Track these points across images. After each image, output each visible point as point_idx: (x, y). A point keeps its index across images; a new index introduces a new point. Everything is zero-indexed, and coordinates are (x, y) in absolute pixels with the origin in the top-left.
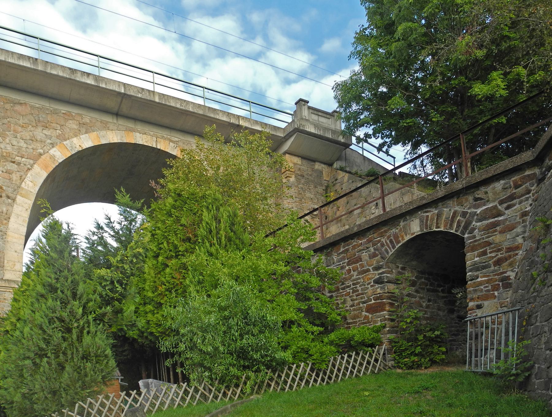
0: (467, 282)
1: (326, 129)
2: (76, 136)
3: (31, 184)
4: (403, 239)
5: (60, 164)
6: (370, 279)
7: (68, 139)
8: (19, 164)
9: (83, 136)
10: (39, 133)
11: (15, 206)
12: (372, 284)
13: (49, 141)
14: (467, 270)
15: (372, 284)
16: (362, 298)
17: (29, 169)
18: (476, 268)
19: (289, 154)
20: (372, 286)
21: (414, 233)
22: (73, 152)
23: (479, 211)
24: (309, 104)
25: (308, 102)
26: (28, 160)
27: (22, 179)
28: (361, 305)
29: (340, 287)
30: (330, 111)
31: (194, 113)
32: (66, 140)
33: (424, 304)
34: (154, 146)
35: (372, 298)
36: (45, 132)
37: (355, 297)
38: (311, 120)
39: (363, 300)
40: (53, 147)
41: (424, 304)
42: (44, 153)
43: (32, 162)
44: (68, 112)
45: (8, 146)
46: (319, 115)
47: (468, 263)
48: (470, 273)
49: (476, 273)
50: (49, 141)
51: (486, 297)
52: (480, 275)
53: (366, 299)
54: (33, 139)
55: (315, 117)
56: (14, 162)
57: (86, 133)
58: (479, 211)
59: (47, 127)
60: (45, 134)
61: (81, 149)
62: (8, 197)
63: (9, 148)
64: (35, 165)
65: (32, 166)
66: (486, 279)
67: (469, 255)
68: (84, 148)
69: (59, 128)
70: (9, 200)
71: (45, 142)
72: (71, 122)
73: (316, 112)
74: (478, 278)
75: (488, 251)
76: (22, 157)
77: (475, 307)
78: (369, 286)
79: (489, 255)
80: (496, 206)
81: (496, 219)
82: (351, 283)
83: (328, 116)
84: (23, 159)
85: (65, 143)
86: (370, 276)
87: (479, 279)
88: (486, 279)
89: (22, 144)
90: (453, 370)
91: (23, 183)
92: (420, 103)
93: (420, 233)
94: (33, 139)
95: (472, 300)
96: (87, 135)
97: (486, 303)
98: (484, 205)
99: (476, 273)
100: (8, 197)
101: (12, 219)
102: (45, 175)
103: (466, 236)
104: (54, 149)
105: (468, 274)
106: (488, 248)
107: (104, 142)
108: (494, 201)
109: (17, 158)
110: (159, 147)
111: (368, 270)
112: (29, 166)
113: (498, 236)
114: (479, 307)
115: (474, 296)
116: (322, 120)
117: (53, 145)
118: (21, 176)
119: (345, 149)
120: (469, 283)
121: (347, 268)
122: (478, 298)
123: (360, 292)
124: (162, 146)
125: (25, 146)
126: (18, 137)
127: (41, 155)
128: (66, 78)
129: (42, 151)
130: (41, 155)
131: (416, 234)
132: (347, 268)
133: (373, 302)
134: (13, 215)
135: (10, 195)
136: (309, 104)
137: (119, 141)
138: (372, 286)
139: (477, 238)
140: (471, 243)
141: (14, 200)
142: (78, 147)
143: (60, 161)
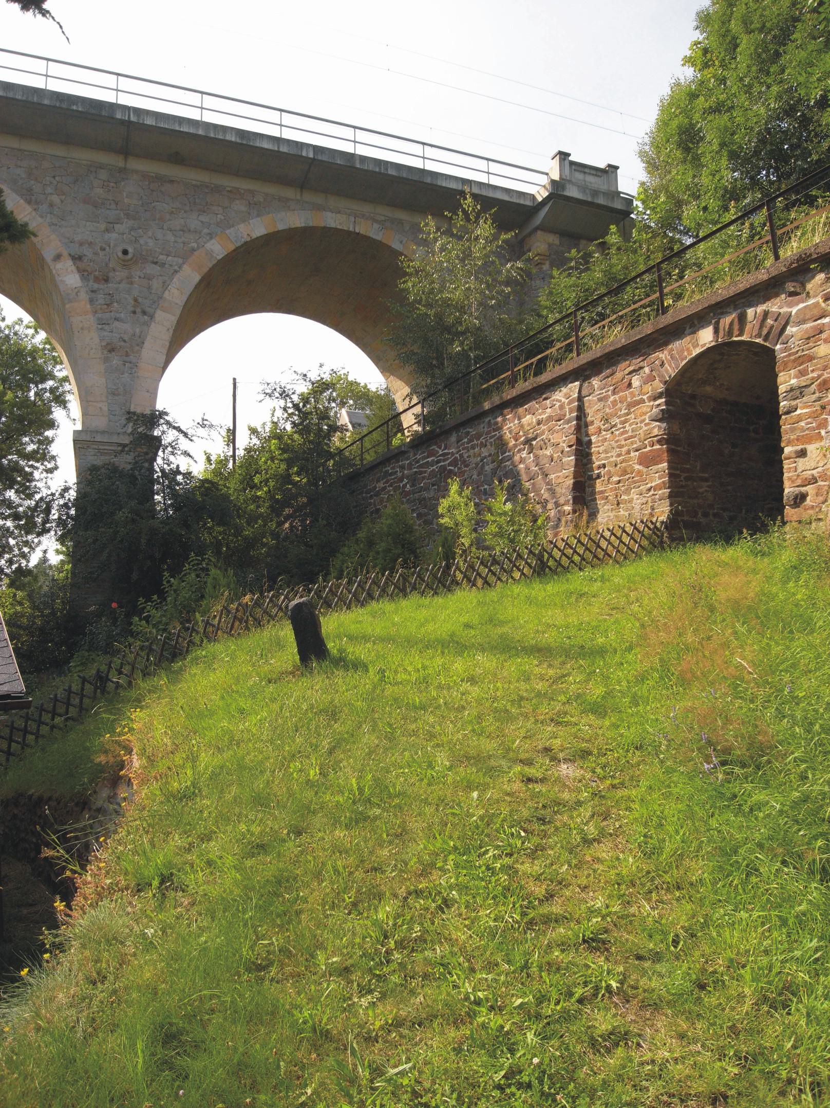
0: (780, 416)
1: (595, 193)
2: (244, 221)
3: (176, 293)
4: (690, 354)
5: (219, 261)
6: (645, 414)
7: (233, 226)
8: (163, 265)
9: (254, 220)
10: (194, 222)
11: (153, 324)
12: (647, 421)
13: (206, 231)
14: (781, 397)
15: (647, 421)
16: (632, 443)
17: (176, 272)
18: (798, 392)
19: (542, 230)
20: (646, 425)
21: (705, 344)
22: (239, 244)
23: (794, 310)
24: (571, 158)
25: (569, 155)
26: (176, 259)
27: (165, 286)
28: (632, 454)
29: (603, 427)
30: (602, 165)
31: (408, 179)
32: (229, 228)
33: (726, 451)
34: (351, 229)
35: (646, 442)
36: (202, 218)
37: (623, 443)
38: (573, 180)
39: (635, 446)
40: (211, 238)
41: (726, 451)
42: (198, 248)
43: (180, 261)
44: (235, 188)
45: (150, 240)
46: (585, 173)
47: (782, 389)
48: (785, 402)
49: (794, 403)
50: (206, 231)
51: (809, 440)
52: (800, 405)
53: (639, 444)
54: (185, 230)
55: (579, 176)
56: (156, 263)
57: (258, 216)
58: (794, 310)
59: (204, 212)
60: (202, 222)
61: (249, 239)
62: (144, 313)
63: (151, 243)
64: (185, 266)
65: (180, 267)
66: (807, 410)
67: (782, 376)
68: (254, 236)
69: (221, 211)
70: (146, 317)
71: (200, 233)
72: (237, 202)
73: (580, 169)
74: (796, 409)
75: (810, 369)
76: (168, 255)
77: (793, 455)
78: (643, 425)
79: (811, 375)
80: (818, 303)
81: (819, 322)
82: (618, 421)
83: (599, 174)
84: (170, 258)
85: (228, 232)
86: (645, 410)
87: (798, 412)
88: (807, 410)
89: (170, 237)
90: (555, 616)
91: (167, 292)
92: (6, 417)
93: (713, 344)
94: (185, 230)
95: (789, 443)
96: (259, 219)
97: (811, 448)
98: (803, 302)
99: (794, 403)
100: (144, 313)
101: (147, 345)
102: (197, 278)
103: (778, 347)
104: (213, 241)
105: (782, 404)
106: (809, 364)
107: (281, 227)
108: (815, 296)
109: (161, 257)
110: (357, 231)
111: (642, 401)
112: (176, 268)
113: (822, 347)
114: (802, 454)
115: (792, 437)
116: (590, 179)
117: (211, 236)
118: (164, 283)
119: (623, 219)
120: (783, 417)
121: (612, 398)
122: (798, 440)
123: (630, 434)
124: (363, 228)
125: (173, 239)
126: (165, 227)
127: (193, 250)
128: (236, 143)
129: (195, 245)
130: (193, 250)
131: (708, 346)
132: (612, 398)
133: (649, 448)
134: (149, 337)
135: (147, 309)
136: (571, 158)
137: (303, 225)
138: (646, 425)
139: (793, 350)
140: (784, 357)
141: (152, 317)
142: (245, 236)
143: (219, 257)
